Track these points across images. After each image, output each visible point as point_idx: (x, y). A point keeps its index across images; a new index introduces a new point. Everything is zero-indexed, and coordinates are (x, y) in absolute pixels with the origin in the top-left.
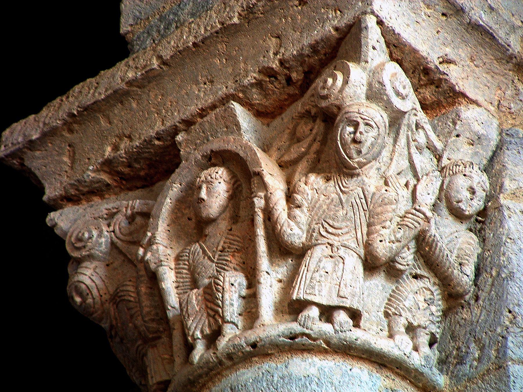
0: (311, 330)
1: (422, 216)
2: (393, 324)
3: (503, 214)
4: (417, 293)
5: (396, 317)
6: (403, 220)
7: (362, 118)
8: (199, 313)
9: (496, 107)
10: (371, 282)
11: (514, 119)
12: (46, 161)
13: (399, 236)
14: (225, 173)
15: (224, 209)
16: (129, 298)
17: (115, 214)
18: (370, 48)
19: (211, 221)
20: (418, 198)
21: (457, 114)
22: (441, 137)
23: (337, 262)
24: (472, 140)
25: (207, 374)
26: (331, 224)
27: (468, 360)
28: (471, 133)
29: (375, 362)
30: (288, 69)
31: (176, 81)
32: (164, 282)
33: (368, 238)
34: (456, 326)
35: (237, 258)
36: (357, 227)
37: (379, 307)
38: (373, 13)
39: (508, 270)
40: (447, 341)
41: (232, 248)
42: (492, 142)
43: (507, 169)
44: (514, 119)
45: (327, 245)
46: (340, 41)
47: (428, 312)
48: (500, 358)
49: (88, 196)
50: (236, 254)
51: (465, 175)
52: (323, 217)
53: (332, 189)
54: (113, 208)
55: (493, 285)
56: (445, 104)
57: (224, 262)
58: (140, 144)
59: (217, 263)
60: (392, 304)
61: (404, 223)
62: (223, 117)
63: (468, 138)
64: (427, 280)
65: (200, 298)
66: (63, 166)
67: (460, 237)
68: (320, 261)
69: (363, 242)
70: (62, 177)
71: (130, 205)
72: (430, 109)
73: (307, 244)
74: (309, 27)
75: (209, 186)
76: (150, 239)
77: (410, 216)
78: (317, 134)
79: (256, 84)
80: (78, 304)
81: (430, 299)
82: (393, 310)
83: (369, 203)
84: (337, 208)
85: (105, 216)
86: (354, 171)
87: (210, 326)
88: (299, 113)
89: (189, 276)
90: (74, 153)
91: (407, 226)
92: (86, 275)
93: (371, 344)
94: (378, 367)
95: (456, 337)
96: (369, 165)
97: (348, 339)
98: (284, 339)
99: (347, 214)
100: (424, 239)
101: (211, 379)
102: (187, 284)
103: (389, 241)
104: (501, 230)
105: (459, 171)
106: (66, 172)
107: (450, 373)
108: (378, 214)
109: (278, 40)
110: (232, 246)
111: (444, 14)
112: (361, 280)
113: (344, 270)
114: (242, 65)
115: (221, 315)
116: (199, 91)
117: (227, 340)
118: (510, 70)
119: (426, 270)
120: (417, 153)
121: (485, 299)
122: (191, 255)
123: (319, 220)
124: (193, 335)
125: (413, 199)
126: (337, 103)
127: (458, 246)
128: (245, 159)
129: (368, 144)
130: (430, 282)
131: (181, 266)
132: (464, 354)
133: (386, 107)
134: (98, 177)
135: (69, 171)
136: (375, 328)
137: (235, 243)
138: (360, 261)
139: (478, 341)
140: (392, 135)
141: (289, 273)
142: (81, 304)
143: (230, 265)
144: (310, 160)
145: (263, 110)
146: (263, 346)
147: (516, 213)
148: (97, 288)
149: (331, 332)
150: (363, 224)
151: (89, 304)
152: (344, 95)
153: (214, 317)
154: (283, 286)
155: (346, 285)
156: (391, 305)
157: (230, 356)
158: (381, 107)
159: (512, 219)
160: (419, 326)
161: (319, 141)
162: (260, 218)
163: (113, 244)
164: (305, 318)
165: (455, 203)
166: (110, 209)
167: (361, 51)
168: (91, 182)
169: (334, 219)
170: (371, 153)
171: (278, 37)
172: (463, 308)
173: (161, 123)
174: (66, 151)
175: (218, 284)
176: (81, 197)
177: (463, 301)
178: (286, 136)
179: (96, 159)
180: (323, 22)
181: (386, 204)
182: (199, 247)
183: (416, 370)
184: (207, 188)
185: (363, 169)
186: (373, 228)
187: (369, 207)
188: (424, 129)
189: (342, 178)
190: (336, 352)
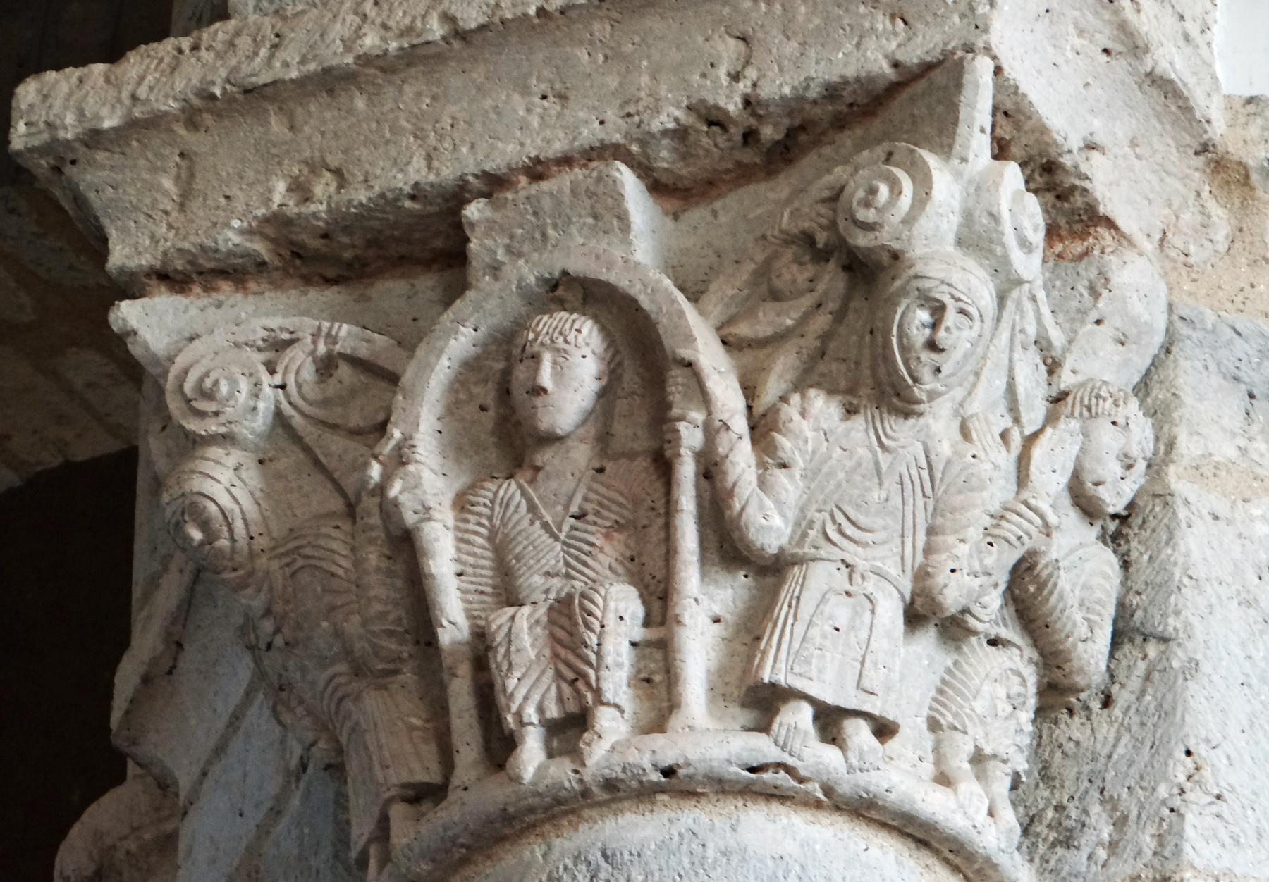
0: (791, 755)
1: (1038, 521)
2: (946, 748)
3: (1174, 513)
5: (958, 735)
6: (998, 526)
7: (953, 297)
8: (535, 666)
11: (1194, 280)
12: (120, 177)
14: (595, 332)
15: (588, 416)
16: (334, 569)
17: (290, 343)
18: (977, 129)
19: (551, 439)
20: (1032, 477)
22: (1061, 318)
25: (547, 809)
26: (852, 517)
27: (1086, 840)
29: (909, 835)
30: (759, 118)
31: (475, 76)
32: (433, 557)
35: (615, 543)
36: (906, 532)
38: (988, 50)
39: (1185, 651)
41: (607, 519)
43: (1182, 404)
44: (1194, 280)
46: (894, 88)
47: (1012, 725)
48: (1167, 858)
49: (209, 278)
50: (615, 534)
51: (1114, 423)
52: (836, 497)
54: (282, 329)
55: (1147, 678)
56: (1064, 233)
57: (586, 548)
58: (370, 199)
59: (564, 543)
60: (948, 703)
62: (591, 194)
63: (1117, 329)
65: (539, 630)
66: (158, 196)
67: (1086, 560)
70: (154, 223)
71: (325, 330)
74: (824, 37)
75: (561, 360)
76: (399, 447)
77: (1015, 518)
79: (674, 131)
80: (195, 544)
81: (1019, 695)
82: (950, 718)
83: (937, 482)
84: (868, 483)
85: (260, 343)
87: (560, 699)
88: (781, 231)
89: (488, 554)
90: (192, 175)
92: (219, 482)
94: (913, 846)
95: (1054, 779)
98: (739, 770)
99: (887, 500)
100: (1031, 568)
101: (553, 817)
102: (484, 572)
104: (1169, 551)
106: (166, 213)
107: (1037, 860)
108: (953, 511)
109: (741, 45)
110: (606, 513)
111: (1106, 51)
114: (645, 80)
115: (594, 684)
116: (528, 110)
117: (607, 747)
118: (1197, 169)
119: (1018, 629)
121: (1128, 708)
122: (497, 508)
123: (825, 502)
124: (518, 714)
126: (896, 245)
128: (653, 316)
130: (1022, 656)
131: (471, 527)
132: (1074, 824)
134: (248, 245)
135: (174, 214)
137: (614, 507)
139: (1110, 803)
141: (738, 603)
142: (202, 544)
143: (601, 556)
144: (804, 351)
145: (670, 182)
147: (1201, 517)
148: (244, 519)
150: (918, 527)
151: (220, 550)
153: (572, 683)
154: (725, 634)
156: (944, 705)
157: (610, 785)
159: (1194, 529)
160: (994, 756)
162: (687, 471)
163: (279, 417)
166: (273, 330)
167: (954, 133)
168: (231, 254)
169: (858, 507)
171: (743, 39)
172: (1071, 712)
173: (423, 163)
174: (172, 164)
175: (590, 614)
176: (194, 276)
177: (1073, 700)
178: (745, 277)
179: (247, 205)
180: (861, 37)
181: (972, 490)
182: (519, 492)
183: (988, 860)
184: (555, 363)
186: (940, 539)
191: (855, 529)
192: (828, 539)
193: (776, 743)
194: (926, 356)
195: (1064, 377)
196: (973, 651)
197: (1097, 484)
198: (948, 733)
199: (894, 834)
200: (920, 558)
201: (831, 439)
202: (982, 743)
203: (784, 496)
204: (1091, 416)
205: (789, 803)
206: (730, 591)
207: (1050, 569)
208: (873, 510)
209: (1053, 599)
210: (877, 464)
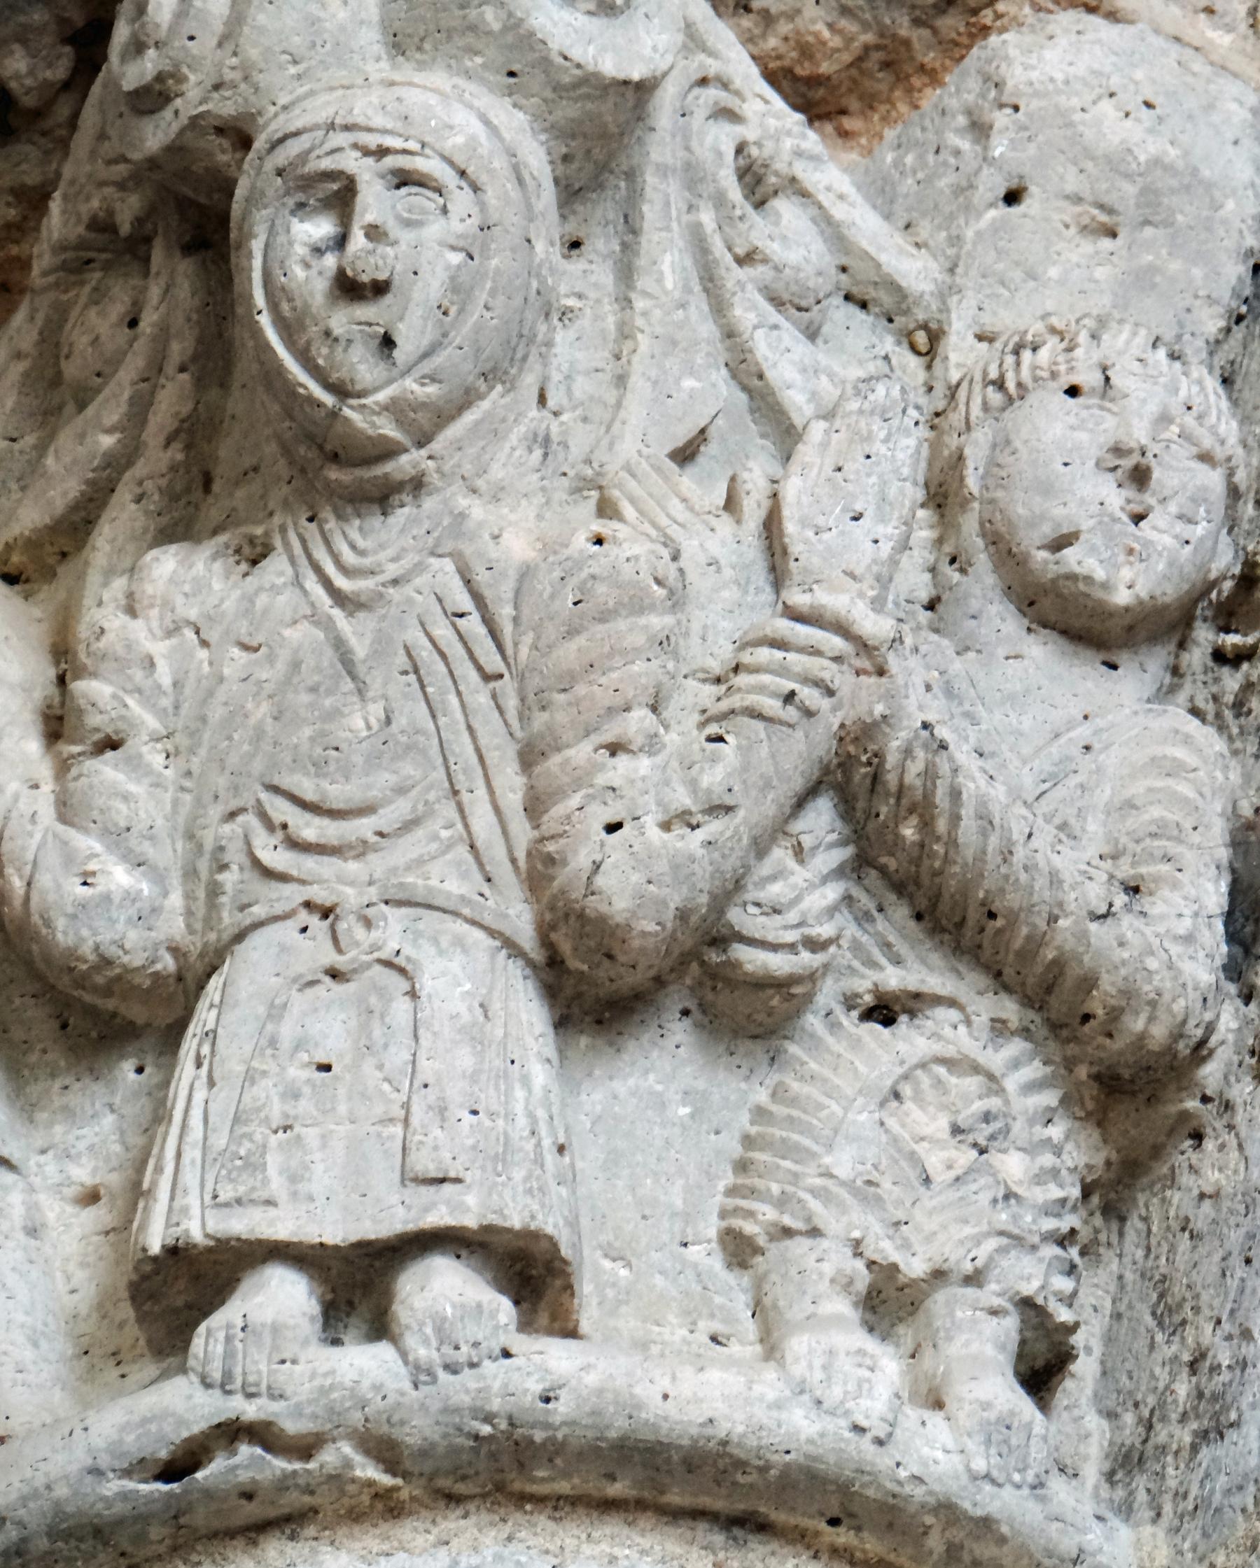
0: (272, 1397)
1: (836, 643)
2: (777, 1292)
4: (897, 1095)
5: (799, 1246)
7: (367, 152)
9: (1243, 27)
10: (620, 1087)
13: (713, 778)
20: (796, 549)
21: (987, 79)
23: (373, 1000)
24: (1102, 207)
26: (310, 796)
28: (1089, 165)
29: (697, 1514)
33: (537, 827)
34: (1172, 1249)
36: (461, 783)
37: (687, 1217)
40: (1141, 1344)
42: (1230, 205)
45: (304, 917)
47: (982, 1192)
51: (1073, 391)
52: (257, 766)
53: (286, 600)
56: (930, 58)
61: (736, 701)
63: (1077, 199)
64: (953, 1015)
68: (276, 1012)
69: (514, 861)
72: (854, 104)
73: (193, 945)
77: (765, 654)
78: (164, 333)
81: (987, 1117)
83: (507, 630)
84: (328, 702)
86: (388, 467)
91: (755, 714)
93: (639, 1406)
94: (718, 1538)
96: (469, 417)
97: (495, 1405)
98: (130, 1485)
99: (388, 721)
100: (876, 778)
103: (661, 817)
105: (1036, 379)
112: (540, 1075)
113: (421, 1032)
119: (935, 958)
120: (776, 327)
123: (236, 789)
125: (773, 569)
126: (225, 107)
127: (1104, 794)
129: (431, 287)
133: (512, 74)
136: (675, 1332)
138: (515, 969)
140: (601, 244)
146: (19, 1553)
149: (391, 1385)
150: (492, 757)
152: (253, 53)
155: (442, 1111)
156: (752, 1192)
158: (483, 81)
160: (939, 1275)
161: (182, 369)
164: (229, 1339)
165: (1043, 555)
169: (319, 767)
170: (463, 334)
177: (1192, 1104)
181: (604, 616)
183: (947, 1510)
185: (436, 446)
186: (554, 761)
187: (510, 651)
188: (804, 194)
189: (331, 524)
190: (453, 1499)
191: (325, 822)
192: (269, 874)
193: (207, 1384)
194: (342, 319)
195: (954, 357)
196: (815, 1043)
197: (1060, 543)
198: (774, 1250)
199: (646, 1521)
200: (523, 833)
201: (213, 636)
202: (888, 1251)
203: (121, 812)
204: (1010, 400)
205: (311, 1531)
206: (109, 1120)
207: (920, 754)
208: (358, 759)
209: (968, 830)
210: (339, 645)
